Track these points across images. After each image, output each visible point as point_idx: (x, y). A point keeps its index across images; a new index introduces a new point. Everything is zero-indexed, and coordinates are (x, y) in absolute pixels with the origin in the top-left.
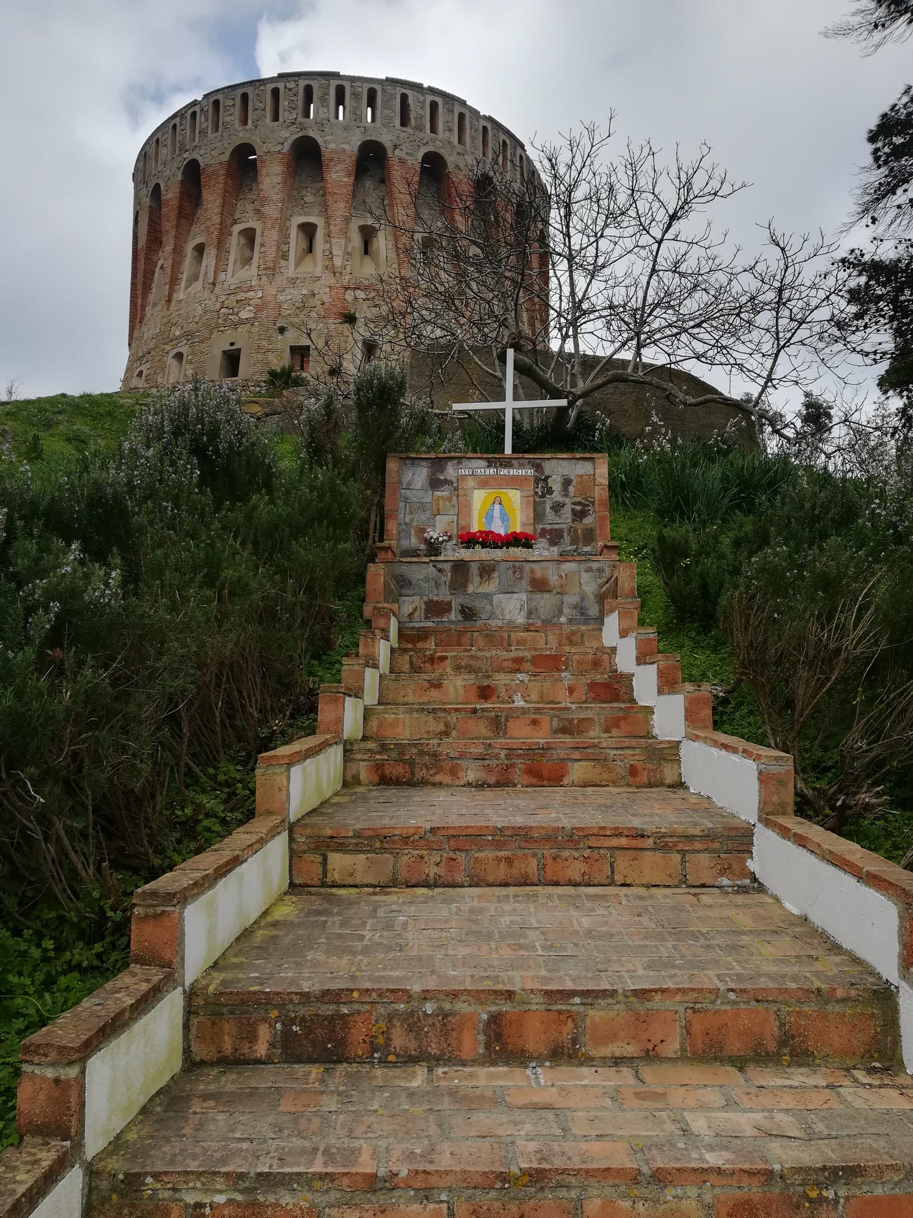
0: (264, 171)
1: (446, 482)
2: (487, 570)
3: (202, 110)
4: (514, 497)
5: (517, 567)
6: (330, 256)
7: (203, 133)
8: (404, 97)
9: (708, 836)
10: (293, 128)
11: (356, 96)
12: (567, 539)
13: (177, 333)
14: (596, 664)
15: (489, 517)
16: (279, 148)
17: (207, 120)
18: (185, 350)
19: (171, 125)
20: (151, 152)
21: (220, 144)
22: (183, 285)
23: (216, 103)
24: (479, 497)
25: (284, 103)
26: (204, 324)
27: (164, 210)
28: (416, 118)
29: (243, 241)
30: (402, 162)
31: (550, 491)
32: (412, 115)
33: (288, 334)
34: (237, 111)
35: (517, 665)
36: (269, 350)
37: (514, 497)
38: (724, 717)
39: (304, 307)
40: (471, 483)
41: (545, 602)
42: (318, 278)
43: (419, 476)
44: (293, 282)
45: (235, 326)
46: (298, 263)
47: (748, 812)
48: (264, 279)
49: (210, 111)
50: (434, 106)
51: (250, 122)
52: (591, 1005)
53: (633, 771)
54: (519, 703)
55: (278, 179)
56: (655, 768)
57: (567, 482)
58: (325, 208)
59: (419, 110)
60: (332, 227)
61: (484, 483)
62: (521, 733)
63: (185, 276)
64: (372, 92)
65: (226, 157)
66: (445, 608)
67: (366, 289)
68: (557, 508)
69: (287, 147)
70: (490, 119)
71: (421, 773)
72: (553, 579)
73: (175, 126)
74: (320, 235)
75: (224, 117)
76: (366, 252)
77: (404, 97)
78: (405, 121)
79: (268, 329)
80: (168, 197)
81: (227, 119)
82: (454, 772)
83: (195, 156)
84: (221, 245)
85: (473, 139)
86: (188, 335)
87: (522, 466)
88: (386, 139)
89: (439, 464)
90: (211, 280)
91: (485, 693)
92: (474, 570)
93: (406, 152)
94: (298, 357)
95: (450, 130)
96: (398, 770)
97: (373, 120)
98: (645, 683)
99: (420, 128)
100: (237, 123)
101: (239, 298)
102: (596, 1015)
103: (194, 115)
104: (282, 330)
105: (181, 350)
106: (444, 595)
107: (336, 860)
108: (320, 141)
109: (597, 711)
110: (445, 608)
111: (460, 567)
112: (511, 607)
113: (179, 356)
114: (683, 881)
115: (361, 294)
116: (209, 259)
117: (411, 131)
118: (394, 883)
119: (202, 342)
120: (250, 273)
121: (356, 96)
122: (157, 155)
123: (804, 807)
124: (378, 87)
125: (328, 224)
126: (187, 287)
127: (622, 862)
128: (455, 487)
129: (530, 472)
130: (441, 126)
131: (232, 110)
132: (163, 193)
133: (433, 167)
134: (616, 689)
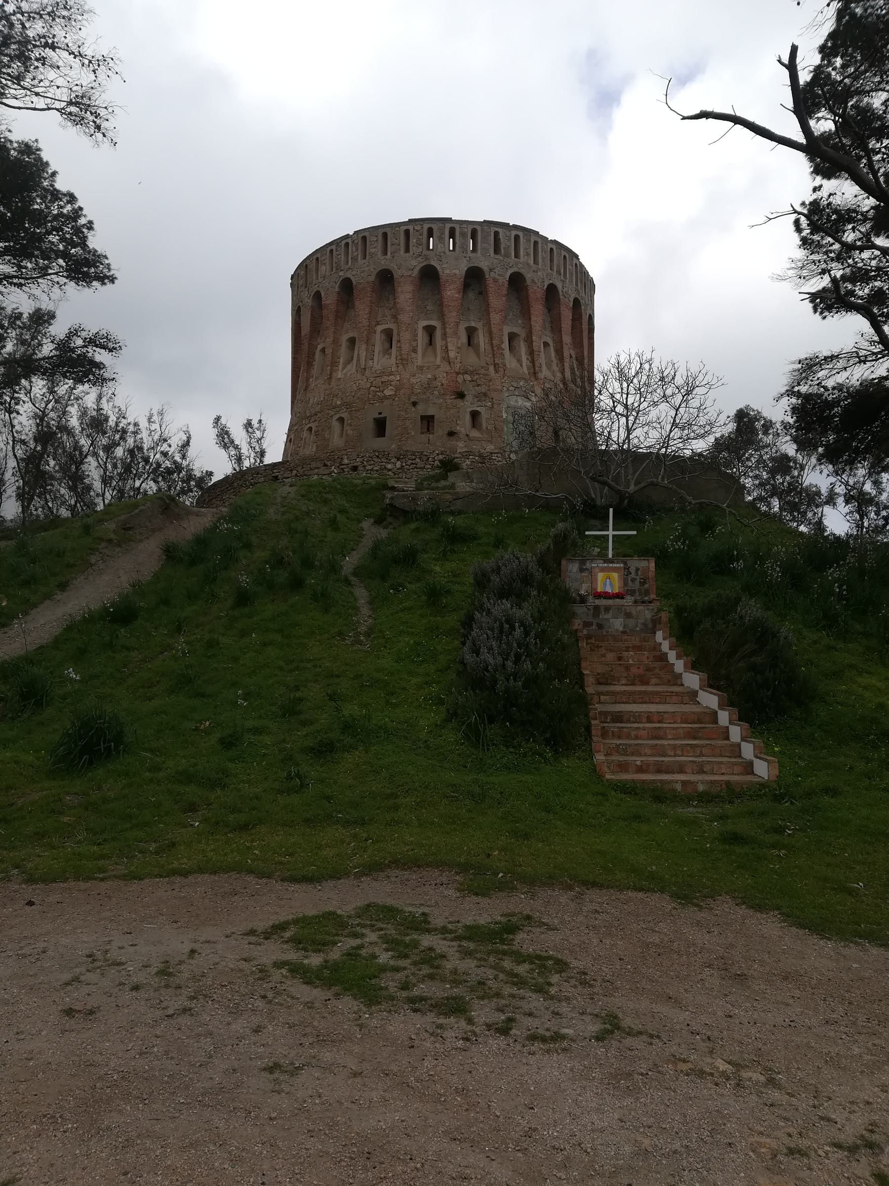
0: (399, 289)
1: (586, 569)
2: (607, 609)
3: (353, 242)
4: (615, 575)
5: (619, 608)
6: (446, 350)
7: (355, 259)
8: (496, 234)
9: (688, 692)
10: (420, 259)
11: (463, 235)
12: (637, 593)
13: (339, 403)
14: (655, 649)
15: (605, 585)
16: (409, 273)
17: (357, 250)
18: (345, 415)
19: (328, 250)
20: (312, 266)
21: (366, 269)
22: (340, 367)
23: (364, 239)
24: (600, 576)
25: (413, 241)
26: (358, 398)
27: (325, 312)
28: (504, 248)
29: (383, 337)
30: (495, 280)
31: (630, 573)
32: (502, 246)
33: (419, 407)
34: (380, 244)
35: (627, 649)
36: (406, 419)
37: (615, 575)
38: (694, 666)
39: (429, 387)
40: (597, 570)
41: (631, 622)
42: (439, 366)
43: (574, 567)
44: (421, 368)
45: (382, 400)
46: (424, 355)
47: (697, 688)
48: (401, 367)
49: (360, 243)
50: (517, 238)
51: (389, 253)
52: (564, 1050)
53: (669, 681)
54: (631, 662)
55: (409, 295)
56: (676, 679)
57: (637, 569)
58: (442, 316)
59: (507, 243)
60: (447, 330)
61: (603, 570)
62: (634, 670)
63: (342, 360)
64: (475, 230)
65: (372, 278)
66: (591, 624)
67: (471, 373)
68: (633, 580)
69: (416, 272)
70: (555, 242)
71: (609, 681)
72: (634, 613)
73: (332, 251)
74: (438, 334)
75: (370, 250)
76: (469, 345)
77: (496, 234)
78: (497, 250)
79: (404, 404)
80: (328, 302)
81: (373, 250)
82: (619, 681)
83: (348, 275)
84: (368, 340)
85: (543, 259)
86: (347, 405)
87: (618, 563)
88: (484, 265)
89: (583, 562)
90: (363, 366)
91: (620, 659)
92: (602, 609)
93: (498, 273)
94: (425, 423)
95: (528, 254)
96: (601, 680)
97: (475, 250)
98: (672, 656)
99: (507, 255)
100: (380, 254)
101: (383, 380)
102: (665, 716)
103: (347, 244)
104: (414, 404)
105: (342, 415)
106: (590, 619)
107: (602, 697)
108: (438, 268)
109: (657, 664)
110: (591, 624)
111: (597, 608)
112: (617, 624)
113: (341, 420)
114: (682, 703)
115: (468, 377)
116: (361, 350)
117: (501, 258)
118: (616, 703)
119: (358, 411)
120: (391, 361)
121: (463, 235)
122: (317, 269)
123: (711, 686)
124: (478, 228)
125: (444, 324)
126: (343, 369)
127: (668, 698)
128: (590, 571)
129: (622, 565)
130: (522, 252)
131: (376, 245)
132: (323, 299)
133: (517, 282)
134: (663, 657)
